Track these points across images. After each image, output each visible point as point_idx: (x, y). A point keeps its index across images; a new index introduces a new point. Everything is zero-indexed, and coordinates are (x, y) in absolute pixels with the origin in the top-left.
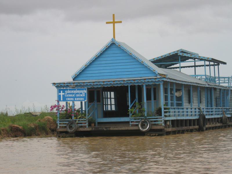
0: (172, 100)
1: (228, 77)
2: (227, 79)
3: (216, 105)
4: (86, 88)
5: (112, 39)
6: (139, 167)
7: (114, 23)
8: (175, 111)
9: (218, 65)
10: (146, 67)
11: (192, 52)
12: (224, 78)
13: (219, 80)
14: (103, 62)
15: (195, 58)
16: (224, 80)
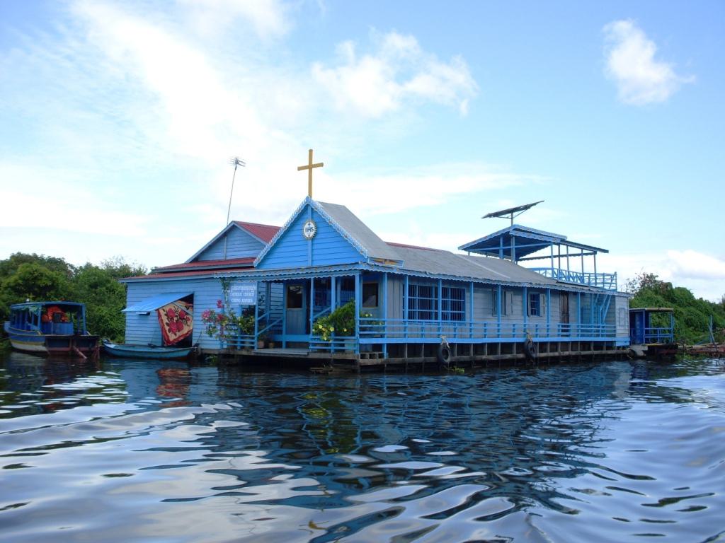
0: (444, 308)
1: (602, 273)
2: (609, 277)
3: (582, 318)
4: (256, 282)
5: (307, 198)
6: (237, 447)
7: (310, 167)
8: (439, 329)
9: (595, 253)
10: (351, 246)
11: (553, 232)
12: (603, 275)
13: (596, 279)
14: (236, 238)
15: (563, 241)
16: (604, 279)
